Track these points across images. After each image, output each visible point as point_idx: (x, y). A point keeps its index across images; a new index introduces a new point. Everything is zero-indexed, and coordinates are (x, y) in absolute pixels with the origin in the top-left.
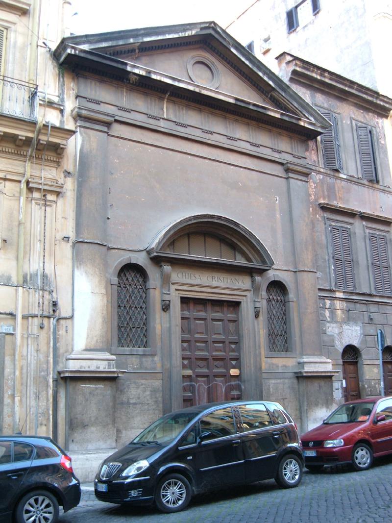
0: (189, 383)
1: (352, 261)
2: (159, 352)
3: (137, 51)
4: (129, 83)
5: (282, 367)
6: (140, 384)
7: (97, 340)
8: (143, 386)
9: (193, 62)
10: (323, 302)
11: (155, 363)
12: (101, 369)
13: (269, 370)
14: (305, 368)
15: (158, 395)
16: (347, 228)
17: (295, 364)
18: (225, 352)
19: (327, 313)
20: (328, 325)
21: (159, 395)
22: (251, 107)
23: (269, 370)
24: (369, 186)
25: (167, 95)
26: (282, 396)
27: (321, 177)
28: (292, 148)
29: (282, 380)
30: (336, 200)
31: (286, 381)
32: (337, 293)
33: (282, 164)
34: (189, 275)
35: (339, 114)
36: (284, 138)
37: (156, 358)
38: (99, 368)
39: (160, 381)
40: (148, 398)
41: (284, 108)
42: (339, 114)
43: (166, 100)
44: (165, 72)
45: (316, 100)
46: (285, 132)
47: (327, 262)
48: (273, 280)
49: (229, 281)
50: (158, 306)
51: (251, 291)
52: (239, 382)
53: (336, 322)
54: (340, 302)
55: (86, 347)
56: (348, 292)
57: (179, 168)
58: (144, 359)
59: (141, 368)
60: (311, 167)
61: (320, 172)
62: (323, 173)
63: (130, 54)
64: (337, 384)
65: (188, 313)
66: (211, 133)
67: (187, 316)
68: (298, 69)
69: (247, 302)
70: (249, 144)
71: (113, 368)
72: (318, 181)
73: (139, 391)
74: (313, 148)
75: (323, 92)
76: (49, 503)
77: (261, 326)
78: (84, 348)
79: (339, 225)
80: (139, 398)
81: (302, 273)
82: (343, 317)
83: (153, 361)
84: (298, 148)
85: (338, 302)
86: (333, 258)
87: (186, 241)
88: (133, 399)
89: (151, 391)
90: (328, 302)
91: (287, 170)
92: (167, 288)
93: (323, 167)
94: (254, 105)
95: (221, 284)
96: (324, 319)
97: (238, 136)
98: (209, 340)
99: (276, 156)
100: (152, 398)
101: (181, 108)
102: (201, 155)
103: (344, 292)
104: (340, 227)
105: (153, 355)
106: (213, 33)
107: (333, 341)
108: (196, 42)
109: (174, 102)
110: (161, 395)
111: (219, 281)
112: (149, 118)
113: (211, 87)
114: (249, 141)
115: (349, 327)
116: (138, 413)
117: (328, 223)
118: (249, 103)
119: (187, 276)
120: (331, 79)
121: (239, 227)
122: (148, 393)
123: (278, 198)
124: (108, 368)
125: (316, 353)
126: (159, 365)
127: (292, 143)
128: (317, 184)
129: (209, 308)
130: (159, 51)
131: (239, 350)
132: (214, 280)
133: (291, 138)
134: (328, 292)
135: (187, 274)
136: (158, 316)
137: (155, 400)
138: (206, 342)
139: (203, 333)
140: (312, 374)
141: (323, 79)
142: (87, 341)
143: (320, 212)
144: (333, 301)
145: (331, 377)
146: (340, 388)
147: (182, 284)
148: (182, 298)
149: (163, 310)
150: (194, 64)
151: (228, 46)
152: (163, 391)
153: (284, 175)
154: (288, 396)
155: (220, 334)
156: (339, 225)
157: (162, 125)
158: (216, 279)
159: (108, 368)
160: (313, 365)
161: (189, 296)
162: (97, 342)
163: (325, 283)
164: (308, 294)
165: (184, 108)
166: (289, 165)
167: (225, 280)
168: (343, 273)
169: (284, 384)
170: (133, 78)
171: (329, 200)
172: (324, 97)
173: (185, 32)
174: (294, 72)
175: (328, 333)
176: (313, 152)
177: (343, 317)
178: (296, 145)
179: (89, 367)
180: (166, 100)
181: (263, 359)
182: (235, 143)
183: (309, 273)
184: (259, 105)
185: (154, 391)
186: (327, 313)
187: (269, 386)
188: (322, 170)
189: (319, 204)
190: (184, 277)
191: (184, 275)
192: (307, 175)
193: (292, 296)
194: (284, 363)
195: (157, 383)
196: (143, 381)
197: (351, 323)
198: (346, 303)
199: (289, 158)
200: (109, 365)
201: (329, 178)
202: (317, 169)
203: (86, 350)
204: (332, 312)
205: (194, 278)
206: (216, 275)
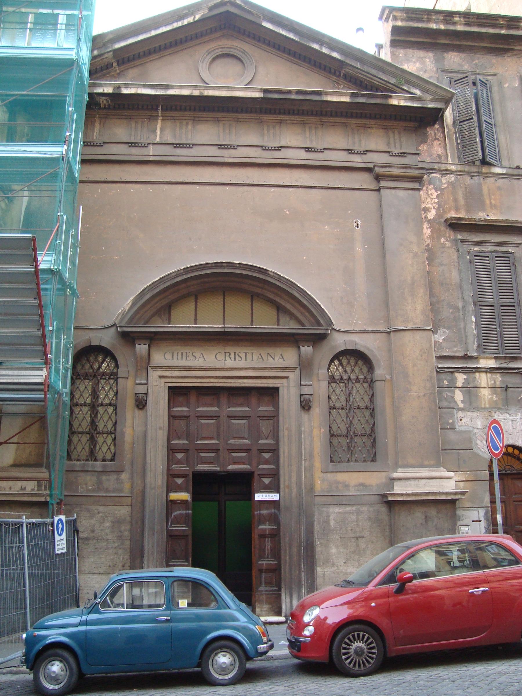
0: (184, 512)
1: (519, 305)
2: (128, 467)
3: (115, 64)
4: (100, 108)
5: (355, 486)
6: (96, 511)
7: (31, 452)
8: (100, 515)
9: (209, 58)
10: (448, 378)
11: (122, 483)
12: (28, 491)
13: (328, 492)
14: (395, 488)
15: (123, 528)
16: (507, 252)
17: (384, 480)
18: (250, 464)
19: (459, 396)
20: (461, 414)
21: (125, 528)
22: (293, 97)
23: (328, 492)
24: (464, 172)
25: (160, 112)
26: (355, 532)
27: (453, 178)
28: (389, 144)
29: (354, 508)
30: (484, 210)
31: (365, 508)
32: (482, 361)
33: (369, 170)
34: (184, 354)
35: (495, 75)
36: (373, 131)
37: (124, 476)
38: (25, 489)
39: (129, 509)
40: (108, 531)
41: (369, 87)
42: (495, 75)
43: (160, 118)
44: (225, 84)
45: (445, 63)
46: (372, 122)
47: (461, 312)
48: (344, 348)
49: (255, 357)
50: (130, 402)
51: (295, 369)
52: (276, 511)
53: (478, 409)
54: (489, 375)
55: (15, 461)
56: (505, 358)
57: (178, 205)
58: (104, 478)
59: (99, 489)
60: (431, 166)
61: (450, 171)
62: (455, 171)
63: (105, 72)
64: (476, 512)
65: (187, 409)
66: (234, 147)
67: (185, 414)
68: (399, 23)
69: (288, 387)
70: (303, 150)
71: (45, 489)
72: (445, 186)
73: (93, 521)
74: (437, 137)
75: (459, 49)
76: (346, 661)
77: (316, 424)
78: (11, 462)
79: (490, 248)
80: (93, 531)
81: (402, 333)
82: (495, 399)
83: (117, 479)
84: (400, 141)
85: (483, 375)
86: (475, 304)
87: (191, 305)
88: (84, 531)
89: (112, 522)
90: (461, 378)
91: (378, 178)
92: (144, 374)
93: (457, 161)
94: (299, 92)
95: (241, 363)
96: (452, 406)
97: (283, 144)
98: (221, 448)
99: (357, 160)
100: (113, 532)
101: (184, 123)
102: (217, 181)
103: (496, 358)
104: (491, 252)
105: (119, 472)
106: (232, 10)
107: (470, 441)
108: (213, 31)
109: (173, 119)
110: (128, 527)
111: (237, 358)
112: (131, 148)
113: (238, 84)
114: (302, 146)
115: (508, 416)
116: (92, 552)
117: (466, 248)
118: (289, 92)
119: (180, 356)
120: (467, 24)
121: (269, 276)
122: (108, 524)
123: (359, 223)
124: (38, 490)
125: (426, 463)
126: (127, 486)
127: (388, 137)
128: (442, 190)
129: (224, 400)
130: (155, 56)
131: (276, 460)
132: (228, 358)
133: (386, 128)
134: (461, 361)
135: (180, 354)
136: (129, 416)
137: (119, 534)
138: (216, 450)
139: (212, 438)
140: (405, 498)
141: (452, 28)
142: (16, 453)
143: (450, 233)
144: (472, 375)
145: (453, 502)
146: (482, 519)
147: (169, 368)
148: (170, 388)
149: (138, 406)
150: (214, 59)
151: (257, 21)
152: (131, 522)
153: (374, 186)
154: (367, 533)
155: (243, 438)
156: (490, 248)
157: (151, 152)
158: (232, 356)
159: (38, 490)
160: (412, 482)
161: (183, 385)
162: (30, 454)
163: (455, 347)
164: (414, 365)
165: (190, 123)
166: (377, 169)
167: (249, 356)
168: (497, 326)
169: (359, 513)
170: (102, 100)
171: (468, 211)
172: (463, 55)
173: (183, 19)
174: (395, 30)
175: (458, 428)
176: (436, 143)
177: (495, 399)
178: (397, 137)
179: (10, 488)
180: (160, 118)
181: (318, 475)
182: (276, 154)
183: (415, 332)
184: (306, 91)
185: (117, 522)
186: (459, 396)
187: (328, 516)
188: (453, 168)
189: (446, 220)
190: (175, 358)
191: (175, 354)
192: (418, 179)
193: (379, 372)
194: (361, 481)
195: (123, 511)
196: (101, 508)
197: (512, 410)
198: (501, 376)
199: (383, 159)
200: (39, 486)
201: (469, 178)
202: (443, 167)
203: (15, 465)
204: (469, 392)
205: (192, 358)
206: (241, 351)
